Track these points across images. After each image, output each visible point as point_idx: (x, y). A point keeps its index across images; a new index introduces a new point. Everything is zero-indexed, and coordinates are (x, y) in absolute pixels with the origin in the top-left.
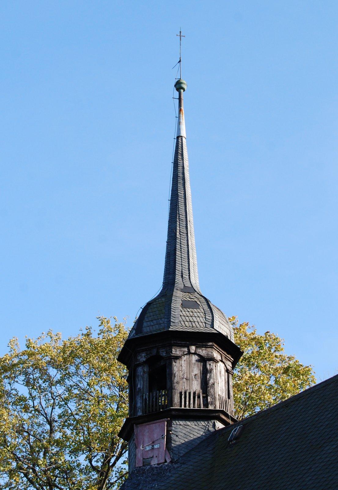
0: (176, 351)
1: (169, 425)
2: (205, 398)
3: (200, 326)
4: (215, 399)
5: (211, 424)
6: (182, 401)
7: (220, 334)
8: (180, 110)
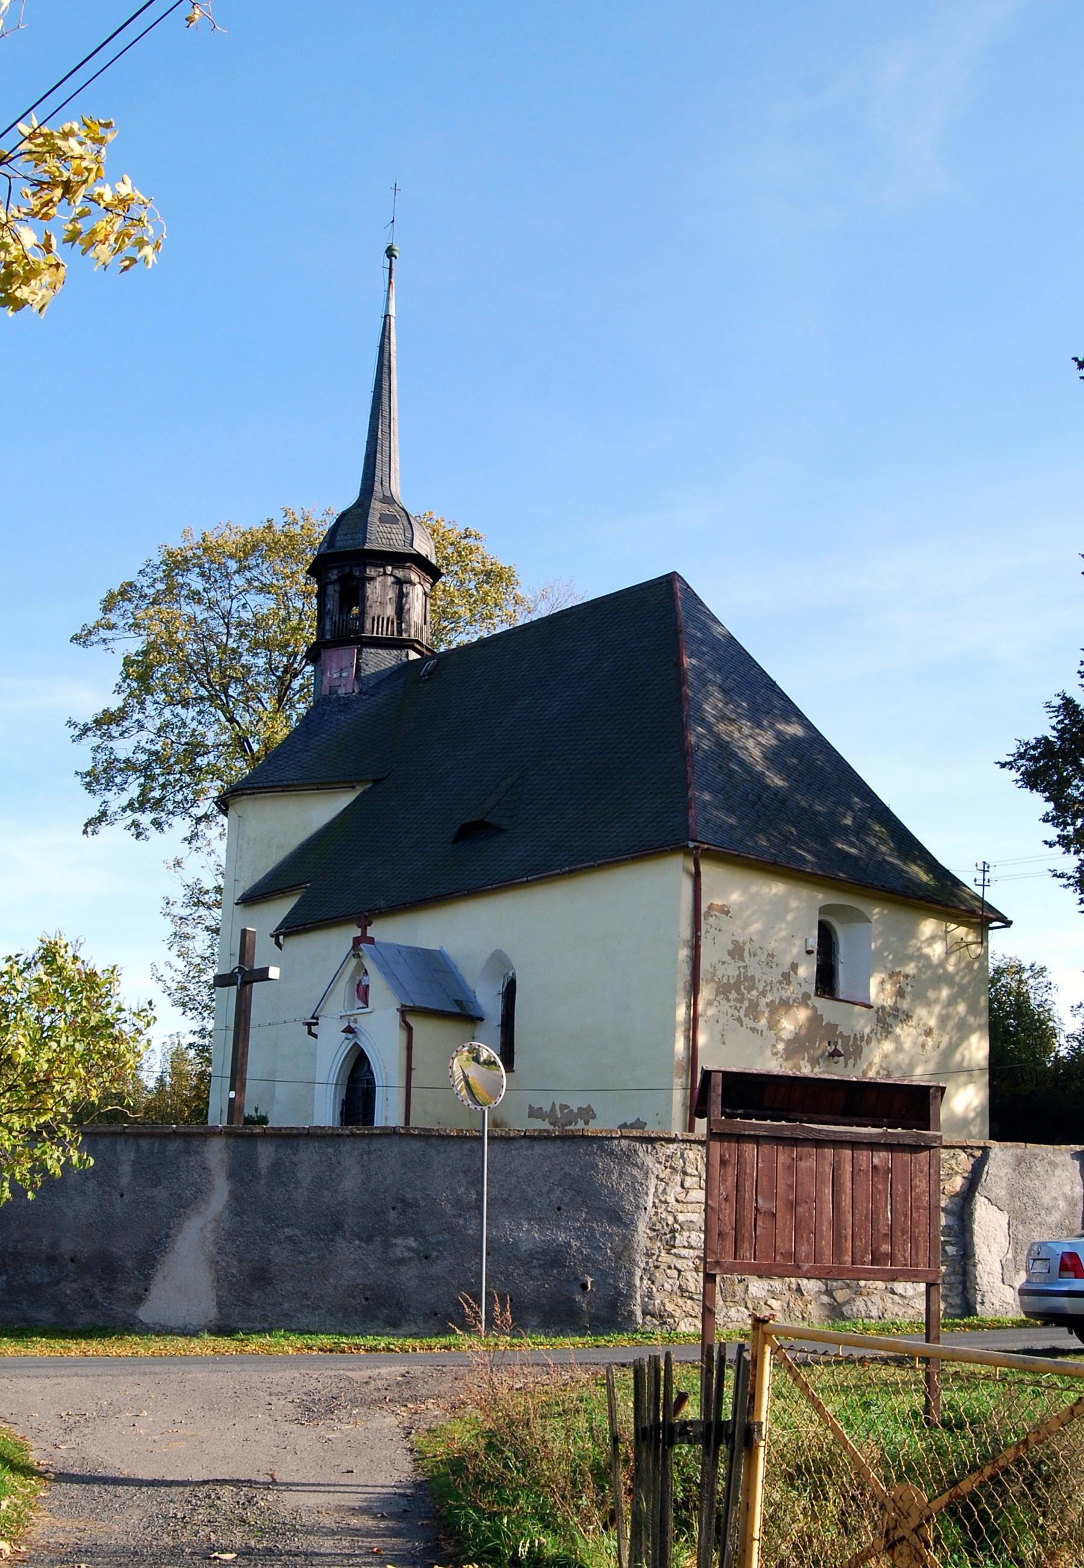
0: (370, 572)
1: (359, 653)
2: (400, 625)
3: (399, 547)
4: (409, 626)
5: (404, 653)
6: (363, 484)
7: (419, 555)
8: (390, 283)
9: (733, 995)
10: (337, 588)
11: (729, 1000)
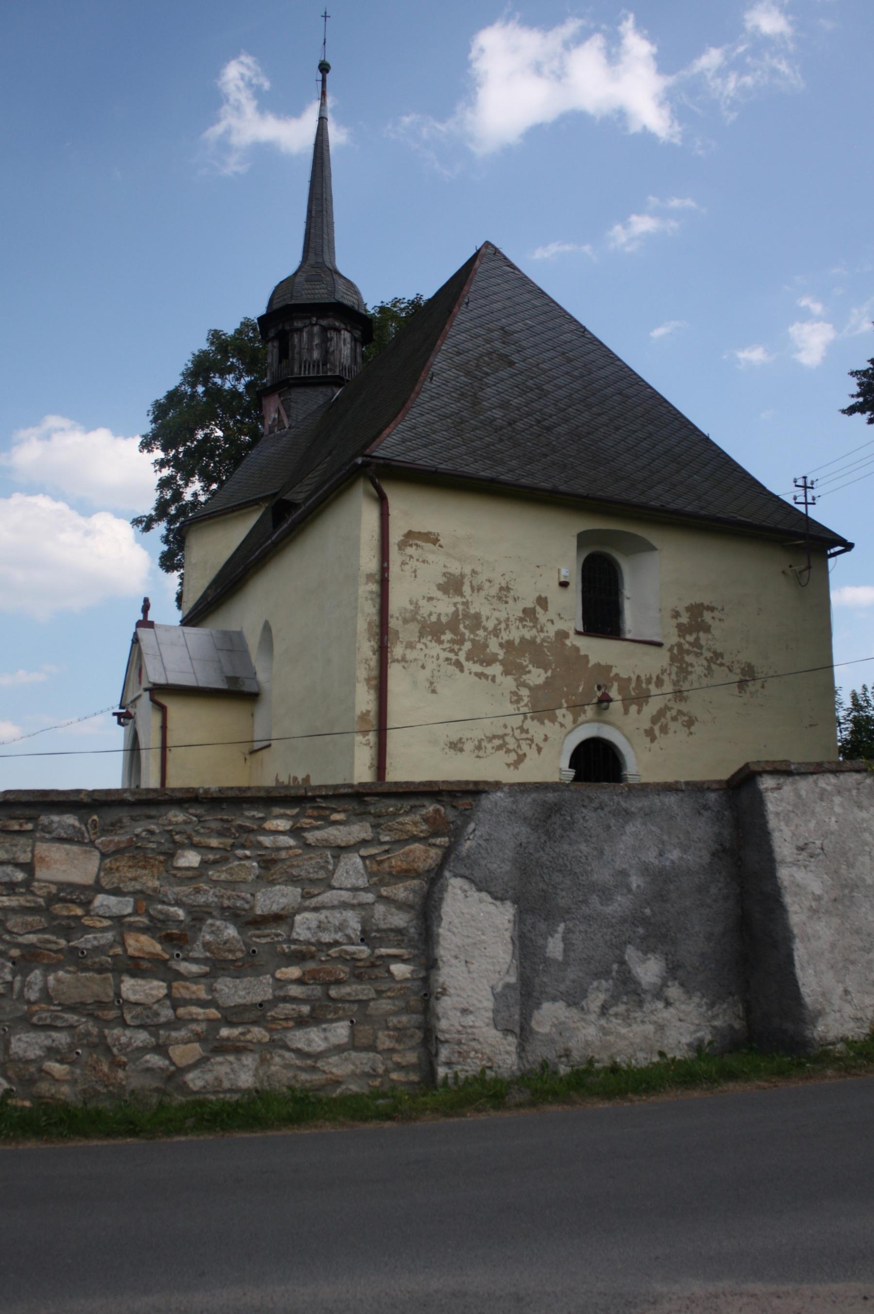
9: (448, 636)
10: (276, 344)
11: (441, 642)
